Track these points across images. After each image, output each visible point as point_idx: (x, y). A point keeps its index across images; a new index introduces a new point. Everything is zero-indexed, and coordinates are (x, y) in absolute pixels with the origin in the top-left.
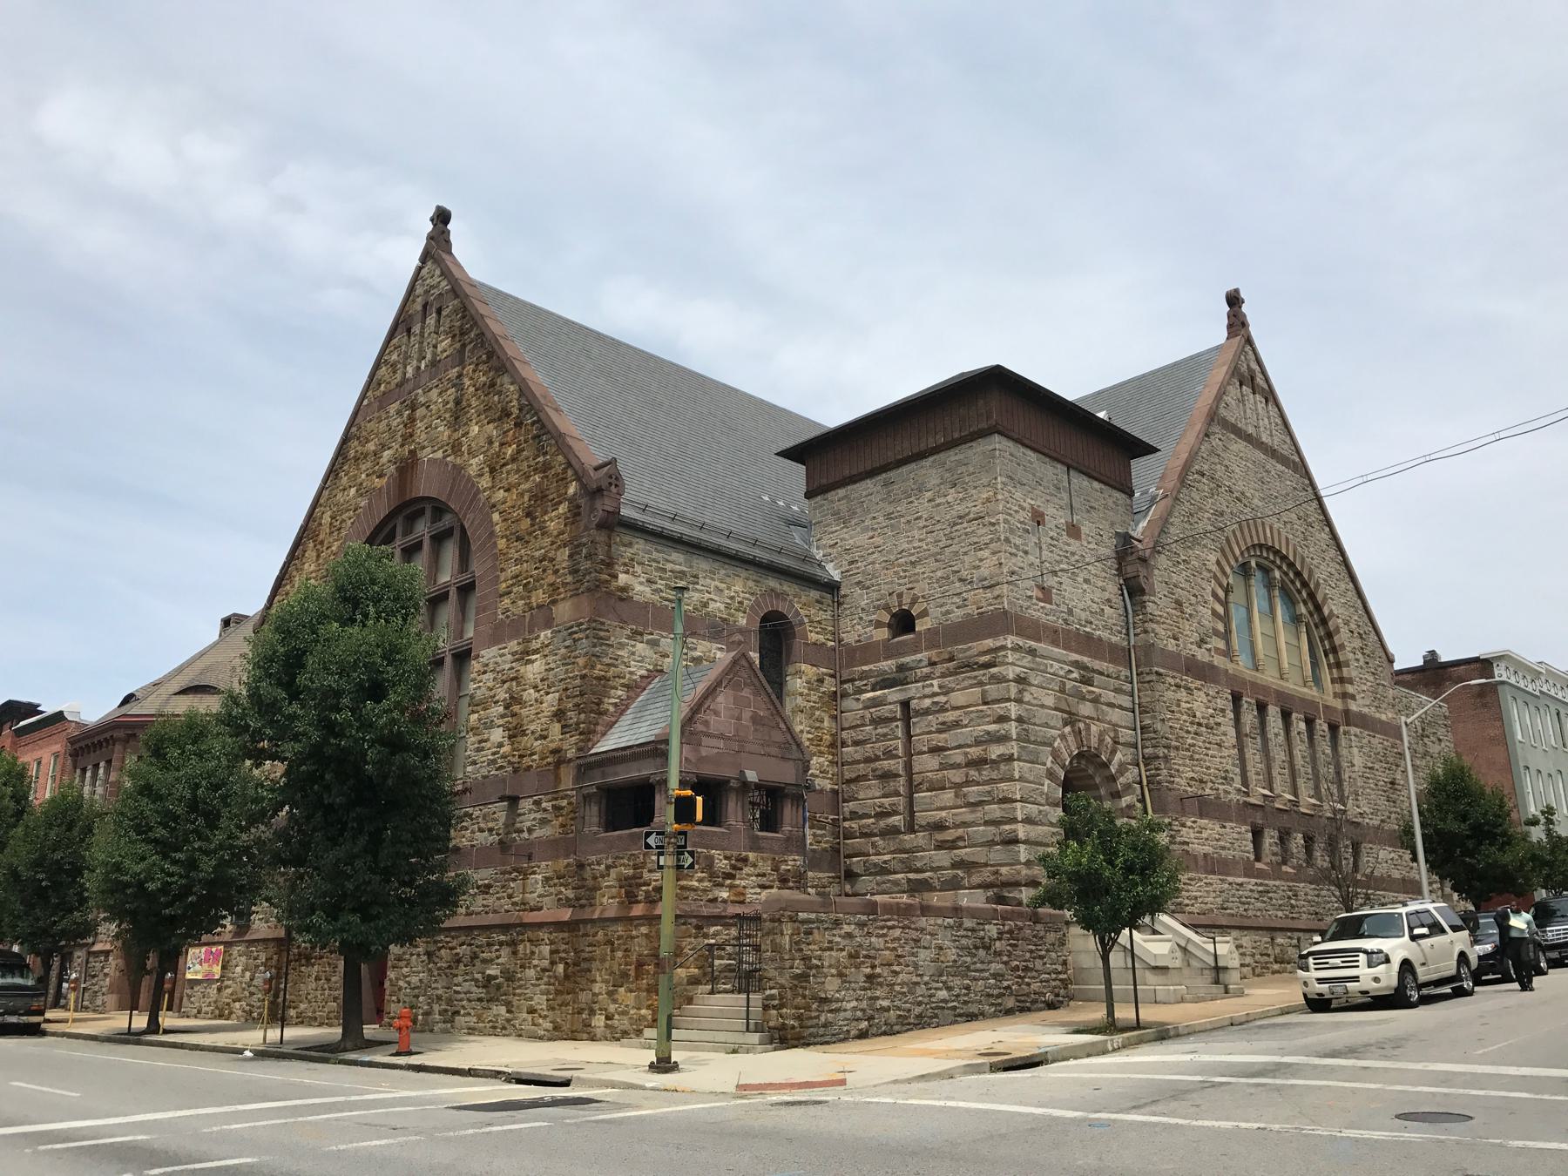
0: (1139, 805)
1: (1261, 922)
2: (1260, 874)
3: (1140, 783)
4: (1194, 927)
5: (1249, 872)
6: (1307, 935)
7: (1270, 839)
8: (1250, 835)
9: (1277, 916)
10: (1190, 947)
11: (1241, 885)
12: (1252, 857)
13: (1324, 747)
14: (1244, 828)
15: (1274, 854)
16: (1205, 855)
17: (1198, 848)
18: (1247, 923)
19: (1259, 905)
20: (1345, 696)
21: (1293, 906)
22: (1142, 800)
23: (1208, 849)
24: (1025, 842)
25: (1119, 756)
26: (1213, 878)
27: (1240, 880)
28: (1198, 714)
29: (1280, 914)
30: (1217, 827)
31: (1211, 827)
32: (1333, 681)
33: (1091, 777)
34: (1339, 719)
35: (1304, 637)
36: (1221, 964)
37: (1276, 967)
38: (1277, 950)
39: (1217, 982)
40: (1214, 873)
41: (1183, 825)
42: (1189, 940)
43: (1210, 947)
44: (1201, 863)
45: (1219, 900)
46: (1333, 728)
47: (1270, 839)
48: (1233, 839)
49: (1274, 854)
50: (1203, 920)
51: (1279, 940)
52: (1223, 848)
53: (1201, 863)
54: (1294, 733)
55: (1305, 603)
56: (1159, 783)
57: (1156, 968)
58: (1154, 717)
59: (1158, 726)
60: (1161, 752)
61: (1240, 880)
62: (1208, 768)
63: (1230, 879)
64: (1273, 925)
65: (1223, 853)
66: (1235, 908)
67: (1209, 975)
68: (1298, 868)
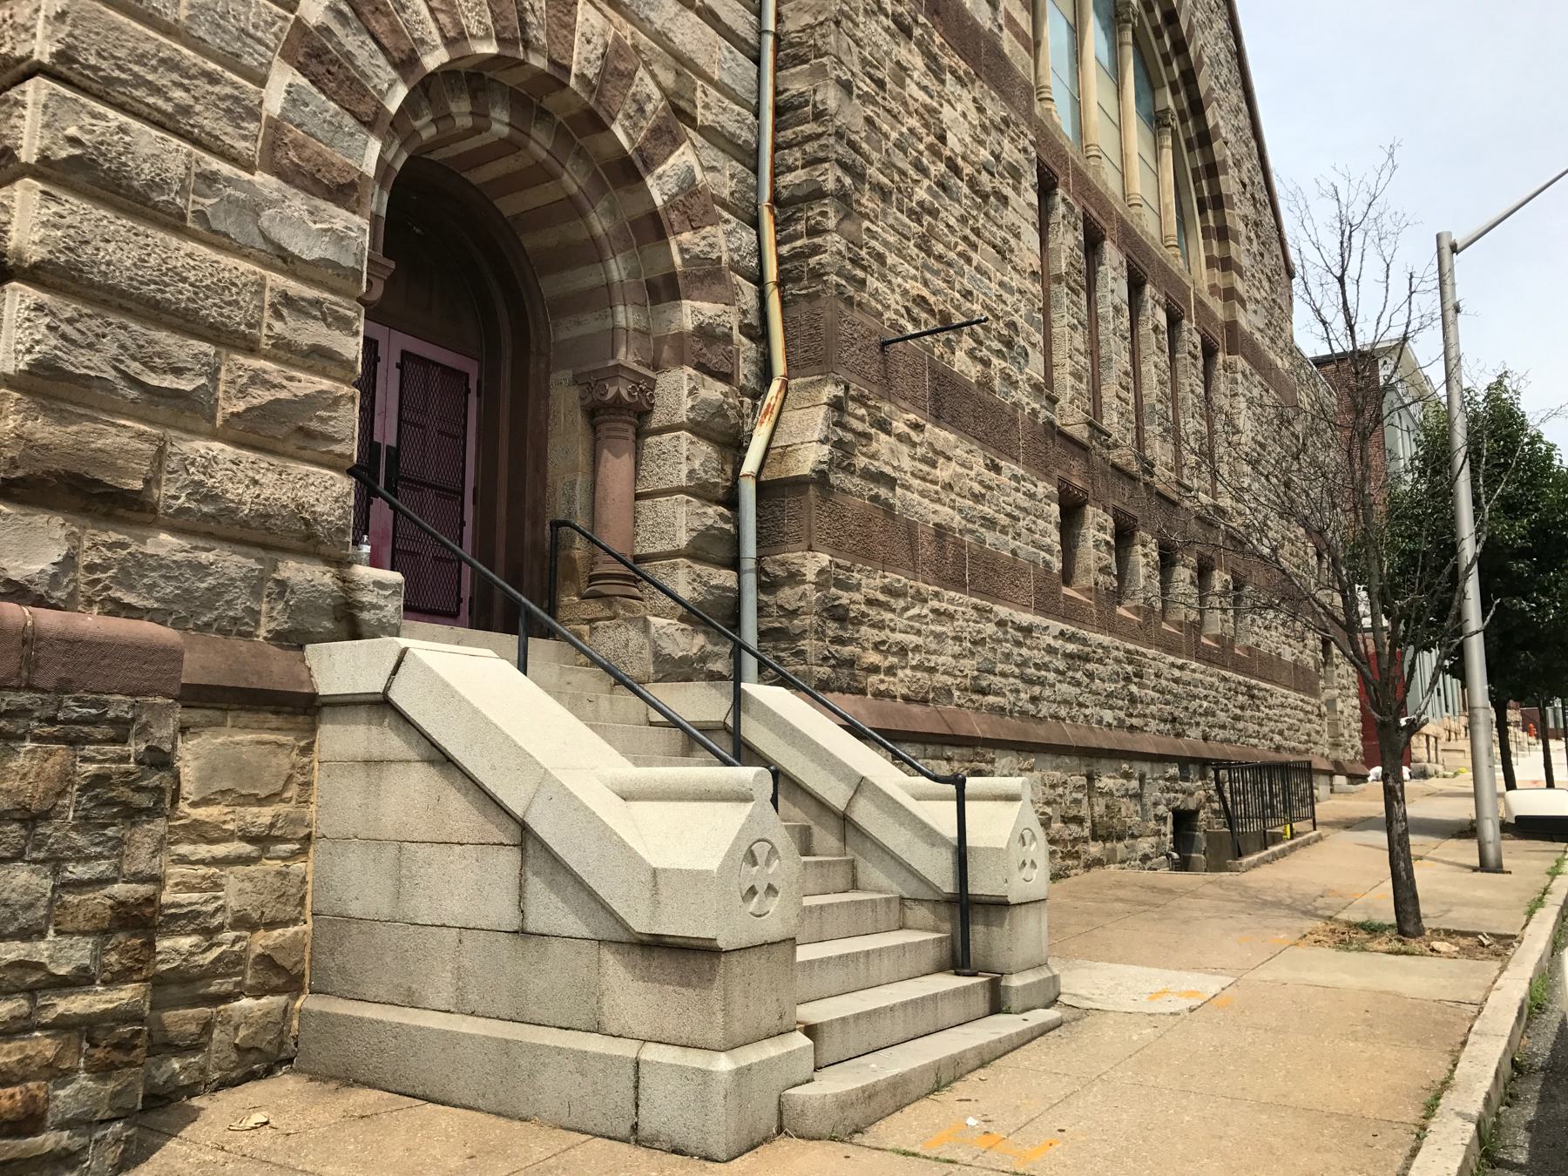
0: (747, 348)
1: (1071, 735)
2: (1070, 612)
3: (759, 280)
4: (890, 740)
5: (1047, 603)
6: (1158, 767)
7: (1096, 526)
8: (1055, 509)
9: (1100, 721)
10: (865, 814)
11: (1027, 630)
12: (1057, 565)
13: (1191, 381)
14: (1042, 488)
15: (1104, 570)
16: (941, 531)
17: (916, 503)
18: (1039, 734)
19: (1065, 689)
20: (1229, 294)
21: (1133, 700)
22: (759, 334)
23: (945, 514)
24: (35, 275)
25: (683, 159)
26: (954, 599)
27: (1026, 618)
28: (951, 139)
29: (1108, 715)
30: (979, 463)
31: (963, 460)
32: (1210, 263)
33: (543, 174)
34: (1220, 339)
35: (1167, 155)
36: (981, 885)
37: (1095, 849)
38: (1099, 809)
39: (958, 960)
40: (958, 584)
41: (884, 426)
42: (861, 785)
43: (942, 816)
44: (927, 550)
45: (969, 665)
46: (1209, 352)
47: (1096, 526)
48: (1015, 507)
49: (1104, 570)
50: (921, 719)
51: (1106, 782)
52: (990, 523)
53: (927, 550)
54: (1145, 329)
55: (1175, 92)
56: (817, 275)
57: (654, 945)
58: (821, 71)
59: (830, 97)
60: (830, 177)
61: (1026, 618)
62: (967, 295)
63: (1002, 611)
64: (1094, 742)
65: (990, 537)
66: (1010, 692)
67: (924, 935)
68: (1147, 611)
